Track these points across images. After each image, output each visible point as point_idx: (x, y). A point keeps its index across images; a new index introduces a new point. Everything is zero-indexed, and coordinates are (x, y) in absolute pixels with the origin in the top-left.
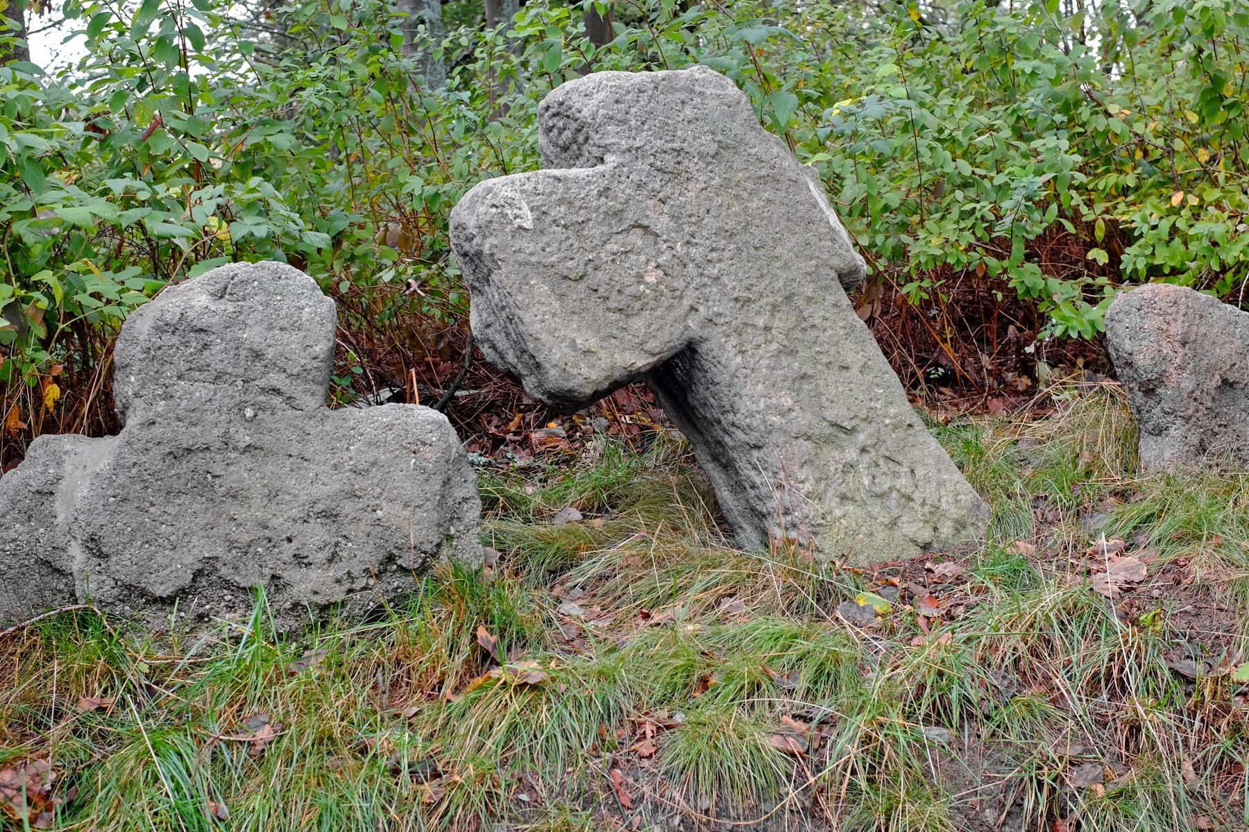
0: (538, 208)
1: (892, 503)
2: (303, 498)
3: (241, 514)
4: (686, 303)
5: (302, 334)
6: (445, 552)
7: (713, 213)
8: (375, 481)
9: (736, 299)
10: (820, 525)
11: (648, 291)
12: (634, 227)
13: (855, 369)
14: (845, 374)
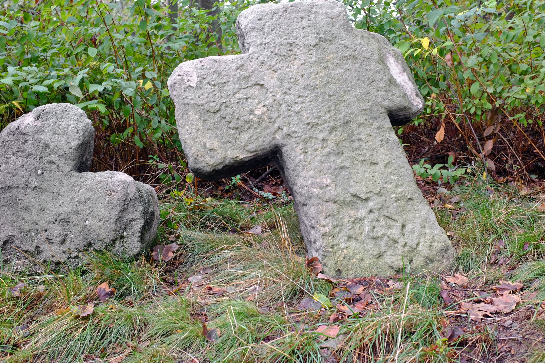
0: (201, 76)
1: (383, 243)
2: (54, 212)
3: (27, 217)
4: (276, 125)
5: (67, 137)
6: (118, 244)
7: (305, 77)
8: (88, 207)
9: (308, 124)
10: (328, 251)
11: (255, 119)
12: (255, 85)
13: (381, 165)
14: (374, 167)
